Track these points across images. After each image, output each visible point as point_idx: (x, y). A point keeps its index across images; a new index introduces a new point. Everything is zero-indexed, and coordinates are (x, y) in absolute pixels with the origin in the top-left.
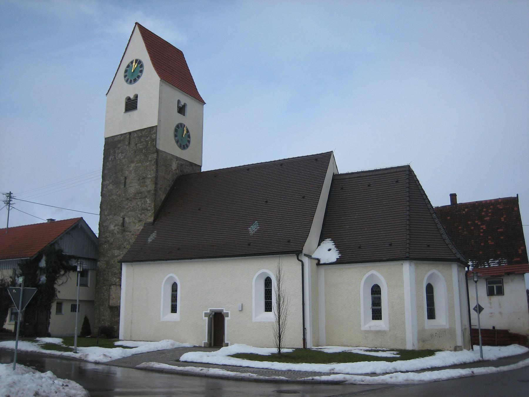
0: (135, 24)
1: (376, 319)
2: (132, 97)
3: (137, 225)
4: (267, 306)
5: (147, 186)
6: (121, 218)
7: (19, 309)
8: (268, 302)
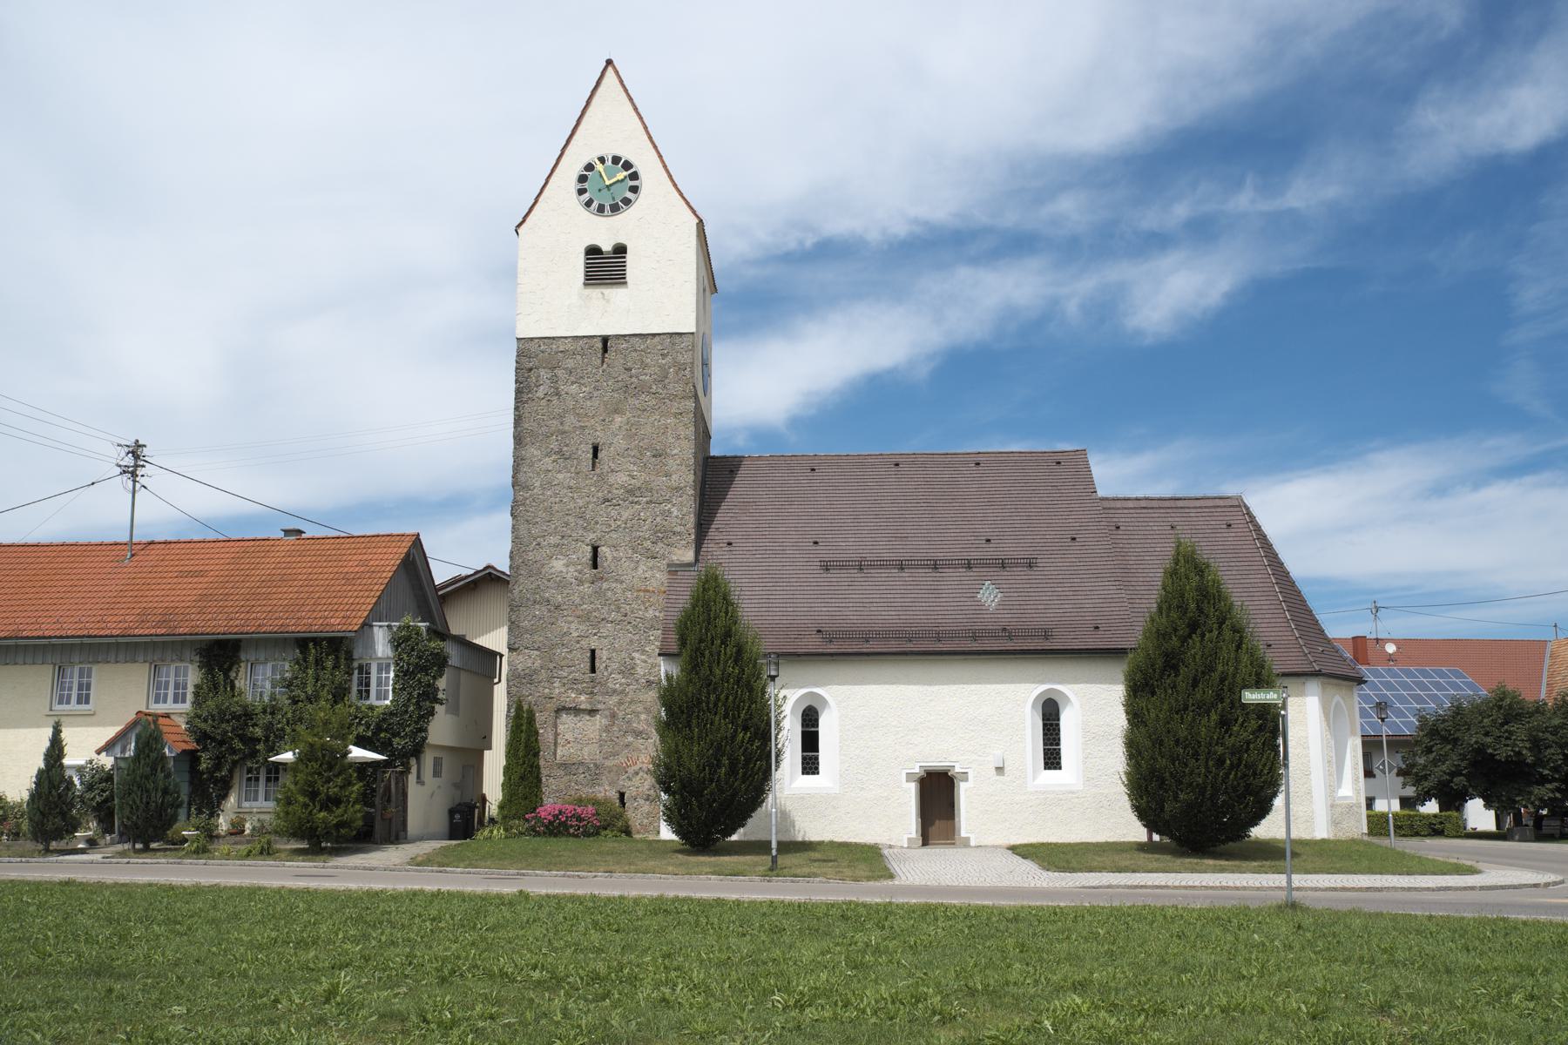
0: (605, 64)
1: (808, 773)
2: (607, 247)
3: (642, 568)
4: (1049, 759)
5: (668, 475)
6: (587, 545)
7: (444, 774)
8: (1049, 750)
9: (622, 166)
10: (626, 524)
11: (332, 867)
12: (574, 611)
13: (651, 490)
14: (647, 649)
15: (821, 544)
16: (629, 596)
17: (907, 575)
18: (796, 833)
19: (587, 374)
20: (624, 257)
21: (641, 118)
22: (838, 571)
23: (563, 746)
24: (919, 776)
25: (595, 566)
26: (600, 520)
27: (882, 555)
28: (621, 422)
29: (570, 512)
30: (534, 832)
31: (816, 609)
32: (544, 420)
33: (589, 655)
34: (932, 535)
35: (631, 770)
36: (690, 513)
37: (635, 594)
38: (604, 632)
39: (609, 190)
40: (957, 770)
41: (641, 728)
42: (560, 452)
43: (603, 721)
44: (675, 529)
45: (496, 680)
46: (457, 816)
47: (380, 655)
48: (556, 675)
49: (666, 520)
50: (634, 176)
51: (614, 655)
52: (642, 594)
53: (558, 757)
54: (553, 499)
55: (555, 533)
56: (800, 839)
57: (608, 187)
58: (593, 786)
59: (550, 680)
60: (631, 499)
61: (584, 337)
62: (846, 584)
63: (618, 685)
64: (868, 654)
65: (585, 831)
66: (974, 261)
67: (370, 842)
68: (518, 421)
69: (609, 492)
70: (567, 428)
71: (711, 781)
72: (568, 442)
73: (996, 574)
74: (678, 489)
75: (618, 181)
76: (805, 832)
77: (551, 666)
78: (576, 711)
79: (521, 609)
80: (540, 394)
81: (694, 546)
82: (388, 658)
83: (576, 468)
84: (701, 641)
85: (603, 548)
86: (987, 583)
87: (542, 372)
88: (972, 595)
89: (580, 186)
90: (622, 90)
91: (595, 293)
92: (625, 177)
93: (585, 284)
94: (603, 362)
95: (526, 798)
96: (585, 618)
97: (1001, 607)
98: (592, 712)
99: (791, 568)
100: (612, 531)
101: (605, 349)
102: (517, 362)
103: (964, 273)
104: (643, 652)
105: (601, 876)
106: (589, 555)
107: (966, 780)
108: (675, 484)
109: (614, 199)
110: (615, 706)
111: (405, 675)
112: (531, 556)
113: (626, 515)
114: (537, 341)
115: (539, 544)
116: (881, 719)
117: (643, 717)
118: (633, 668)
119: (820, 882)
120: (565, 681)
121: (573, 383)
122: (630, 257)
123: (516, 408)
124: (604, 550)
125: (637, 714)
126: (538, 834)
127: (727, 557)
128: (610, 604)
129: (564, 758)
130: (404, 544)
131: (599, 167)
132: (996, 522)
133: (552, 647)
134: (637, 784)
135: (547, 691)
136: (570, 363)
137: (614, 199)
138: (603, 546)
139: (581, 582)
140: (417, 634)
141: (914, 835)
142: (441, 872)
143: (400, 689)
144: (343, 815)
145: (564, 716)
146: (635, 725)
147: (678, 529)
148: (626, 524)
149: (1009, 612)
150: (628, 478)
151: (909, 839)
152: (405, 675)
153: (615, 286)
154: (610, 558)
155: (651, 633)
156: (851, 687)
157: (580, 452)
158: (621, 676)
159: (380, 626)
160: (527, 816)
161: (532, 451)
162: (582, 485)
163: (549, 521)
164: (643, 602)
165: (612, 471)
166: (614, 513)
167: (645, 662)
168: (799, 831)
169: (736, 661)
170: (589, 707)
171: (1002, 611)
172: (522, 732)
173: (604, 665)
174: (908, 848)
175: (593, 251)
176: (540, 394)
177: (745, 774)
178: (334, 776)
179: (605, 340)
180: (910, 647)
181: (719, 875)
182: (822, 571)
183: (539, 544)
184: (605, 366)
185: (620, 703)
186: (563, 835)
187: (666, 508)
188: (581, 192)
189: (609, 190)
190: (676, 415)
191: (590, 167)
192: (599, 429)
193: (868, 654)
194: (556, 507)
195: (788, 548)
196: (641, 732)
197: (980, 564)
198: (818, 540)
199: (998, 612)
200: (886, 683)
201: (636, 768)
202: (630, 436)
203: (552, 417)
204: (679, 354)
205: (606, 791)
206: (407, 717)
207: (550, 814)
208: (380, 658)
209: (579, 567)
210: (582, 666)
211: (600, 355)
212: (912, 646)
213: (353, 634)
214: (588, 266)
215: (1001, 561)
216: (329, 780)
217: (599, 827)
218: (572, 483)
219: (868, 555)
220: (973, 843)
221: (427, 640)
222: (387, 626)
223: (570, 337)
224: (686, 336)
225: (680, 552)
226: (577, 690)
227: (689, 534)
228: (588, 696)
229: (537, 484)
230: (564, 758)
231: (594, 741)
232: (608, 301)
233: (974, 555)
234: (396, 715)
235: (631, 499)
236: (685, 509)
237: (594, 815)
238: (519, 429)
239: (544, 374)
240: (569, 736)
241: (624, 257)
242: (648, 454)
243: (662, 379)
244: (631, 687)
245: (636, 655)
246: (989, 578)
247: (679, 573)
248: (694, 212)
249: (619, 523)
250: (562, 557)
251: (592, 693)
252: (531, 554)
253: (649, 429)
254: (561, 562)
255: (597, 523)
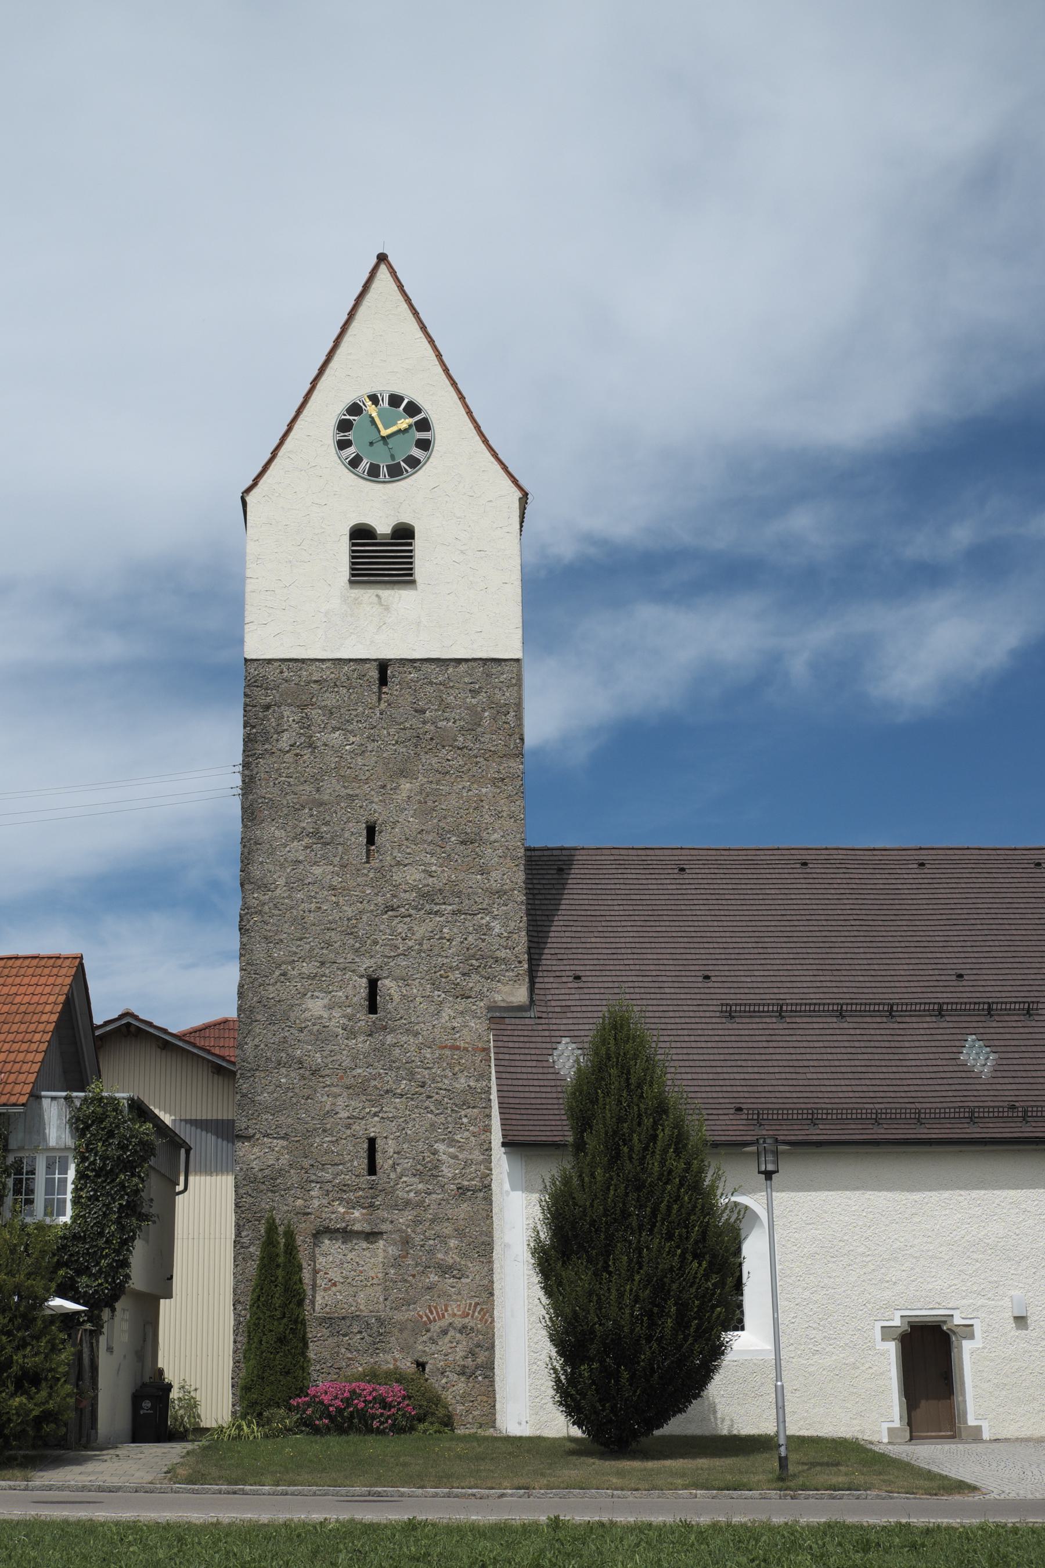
0: (374, 260)
2: (383, 527)
3: (447, 1012)
6: (361, 977)
9: (404, 410)
10: (421, 944)
11: (42, 1488)
12: (342, 1078)
13: (459, 894)
14: (457, 1137)
15: (713, 979)
16: (428, 1056)
17: (851, 1025)
18: (719, 1422)
19: (356, 716)
20: (410, 544)
21: (431, 341)
22: (747, 1020)
23: (325, 1290)
24: (900, 1331)
25: (373, 1008)
26: (381, 938)
27: (807, 996)
28: (411, 791)
29: (333, 926)
30: (308, 1426)
31: (726, 1076)
32: (290, 785)
33: (366, 1146)
34: (876, 967)
35: (435, 1328)
36: (519, 929)
37: (437, 1052)
38: (389, 1111)
39: (386, 444)
40: (957, 1321)
41: (451, 1261)
42: (316, 834)
43: (390, 1249)
44: (498, 954)
45: (180, 1188)
46: (147, 1404)
47: (52, 1142)
48: (313, 1178)
49: (483, 941)
50: (424, 425)
51: (405, 1146)
52: (448, 1052)
53: (317, 1307)
54: (305, 906)
55: (311, 957)
56: (725, 1432)
57: (384, 439)
58: (376, 1351)
59: (304, 1187)
60: (428, 907)
61: (351, 660)
62: (764, 1038)
63: (412, 1195)
64: (819, 1144)
65: (393, 1425)
66: (664, 597)
67: (86, 1448)
68: (249, 784)
69: (394, 896)
70: (326, 797)
71: (649, 1339)
72: (328, 818)
73: (980, 1024)
74: (500, 893)
75: (399, 431)
76: (732, 1420)
77: (306, 1163)
78: (346, 1234)
79: (257, 1074)
80: (284, 745)
81: (527, 980)
82: (67, 1149)
83: (341, 858)
84: (620, 1120)
85: (387, 982)
86: (970, 1038)
87: (287, 712)
88: (952, 1056)
89: (340, 436)
90: (401, 298)
91: (367, 595)
92: (410, 426)
93: (351, 582)
94: (380, 699)
95: (288, 1373)
96: (359, 1089)
97: (999, 1074)
98: (372, 1236)
99: (677, 1014)
100: (399, 955)
101: (383, 681)
102: (246, 695)
103: (648, 613)
104: (452, 1143)
105: (512, 1495)
106: (364, 992)
107: (971, 1336)
108: (496, 886)
109: (393, 457)
110: (408, 1226)
111: (98, 1176)
112: (271, 992)
113: (420, 931)
114: (277, 664)
115: (284, 974)
116: (842, 1244)
117: (453, 1243)
118: (436, 1168)
119: (878, 1497)
120: (329, 1186)
121: (335, 729)
122: (420, 546)
123: (246, 765)
124: (387, 985)
125: (443, 1239)
126: (317, 1431)
127: (577, 997)
128: (398, 1068)
129: (327, 1309)
130: (63, 971)
131: (371, 409)
132: (965, 949)
133: (309, 1133)
134: (445, 1349)
135: (299, 1202)
136: (330, 699)
137: (393, 457)
138: (385, 978)
139: (352, 1034)
140: (115, 1110)
141: (897, 1424)
142: (235, 1493)
143: (89, 1198)
144: (47, 1402)
145: (327, 1242)
146: (440, 1256)
147: (502, 954)
148: (421, 944)
149: (1011, 1080)
150: (423, 875)
151: (890, 1430)
152: (98, 1176)
153: (396, 586)
154: (397, 998)
155: (463, 1113)
156: (793, 1194)
157: (347, 834)
158: (416, 1180)
159: (53, 1098)
160: (294, 1402)
161: (272, 831)
162: (352, 883)
163: (301, 939)
164: (451, 1066)
165: (398, 863)
166: (401, 928)
167: (455, 1157)
168: (723, 1420)
169: (678, 1152)
170: (367, 1228)
171: (1001, 1081)
172: (278, 1266)
173: (390, 1162)
174: (889, 1443)
175: (361, 534)
176: (284, 745)
177: (699, 1327)
178: (33, 1337)
179: (383, 666)
180: (879, 1132)
181: (707, 1489)
182: (724, 1020)
183: (284, 974)
184: (383, 705)
185: (417, 1222)
186: (359, 1431)
187: (484, 921)
188: (343, 445)
189: (386, 444)
190: (494, 782)
191: (355, 409)
192: (376, 800)
193: (819, 1144)
194: (311, 918)
195: (666, 985)
196: (450, 1267)
197: (956, 1010)
198: (709, 974)
199: (996, 1081)
200: (846, 1188)
201: (444, 1323)
202: (425, 813)
203: (302, 779)
204: (497, 691)
205: (396, 1360)
206: (101, 1242)
207: (336, 1398)
208: (53, 1149)
209: (349, 1010)
210: (355, 1163)
211: (375, 689)
212: (883, 1131)
213: (21, 1109)
214: (354, 555)
215: (986, 1007)
216: (23, 1345)
217: (413, 1418)
218: (336, 881)
219: (787, 996)
220: (986, 1436)
221: (129, 1120)
222: (66, 1098)
223: (329, 660)
224: (508, 663)
225: (506, 989)
226: (348, 1201)
227: (520, 962)
228: (364, 1211)
229: (281, 882)
230: (327, 1309)
231: (375, 1281)
232: (387, 609)
233: (943, 997)
234: (83, 1239)
235: (428, 907)
236: (512, 924)
237: (404, 1398)
238: (250, 797)
239: (289, 714)
240: (334, 1274)
241: (410, 544)
242: (453, 839)
243: (473, 727)
244: (434, 1196)
245: (441, 1147)
246: (972, 1031)
247: (507, 1021)
248: (515, 481)
249: (410, 943)
250: (321, 995)
251: (372, 1205)
252: (271, 988)
253: (453, 801)
254: (320, 1003)
255: (375, 943)
